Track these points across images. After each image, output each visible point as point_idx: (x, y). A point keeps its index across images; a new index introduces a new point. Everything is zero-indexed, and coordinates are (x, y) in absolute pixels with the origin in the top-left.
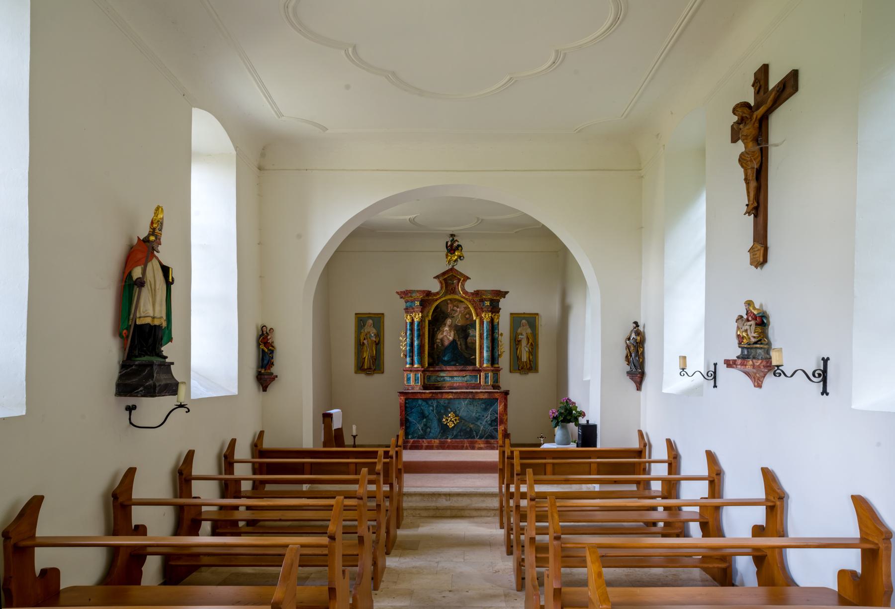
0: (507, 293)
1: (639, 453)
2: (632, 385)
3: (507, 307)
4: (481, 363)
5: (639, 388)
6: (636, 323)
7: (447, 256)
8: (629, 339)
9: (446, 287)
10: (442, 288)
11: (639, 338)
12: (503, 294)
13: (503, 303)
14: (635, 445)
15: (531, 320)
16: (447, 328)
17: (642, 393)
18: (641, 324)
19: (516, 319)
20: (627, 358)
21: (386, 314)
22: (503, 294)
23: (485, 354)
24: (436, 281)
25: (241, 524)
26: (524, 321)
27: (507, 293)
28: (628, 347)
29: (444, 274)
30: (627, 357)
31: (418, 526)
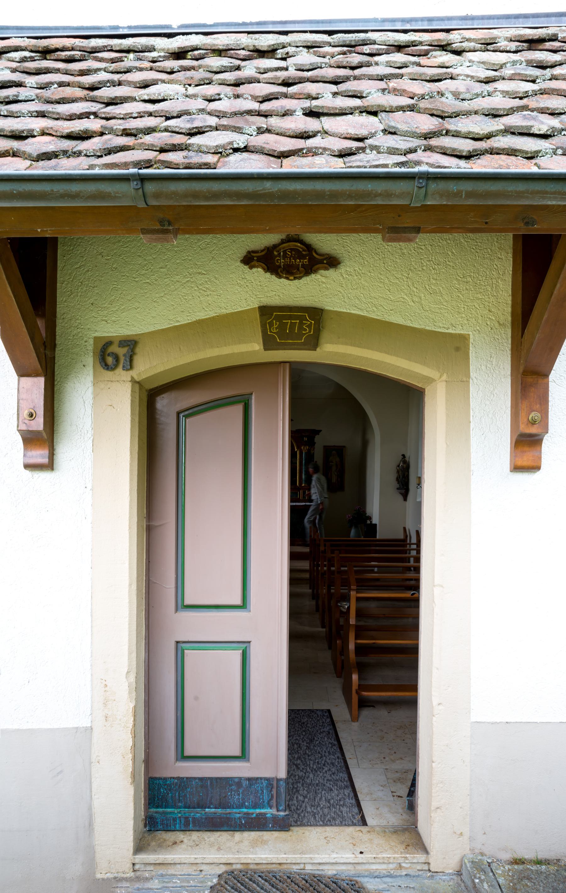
0: (321, 431)
1: (405, 540)
2: (401, 498)
3: (320, 442)
4: (301, 483)
5: (405, 499)
6: (403, 455)
8: (399, 466)
11: (405, 466)
12: (318, 432)
13: (317, 439)
14: (402, 537)
15: (340, 451)
17: (407, 503)
18: (407, 456)
19: (328, 450)
20: (397, 479)
22: (318, 432)
23: (303, 477)
24: (455, 88)
25: (343, 657)
26: (334, 452)
27: (321, 431)
28: (398, 472)
30: (397, 478)
31: (406, 573)
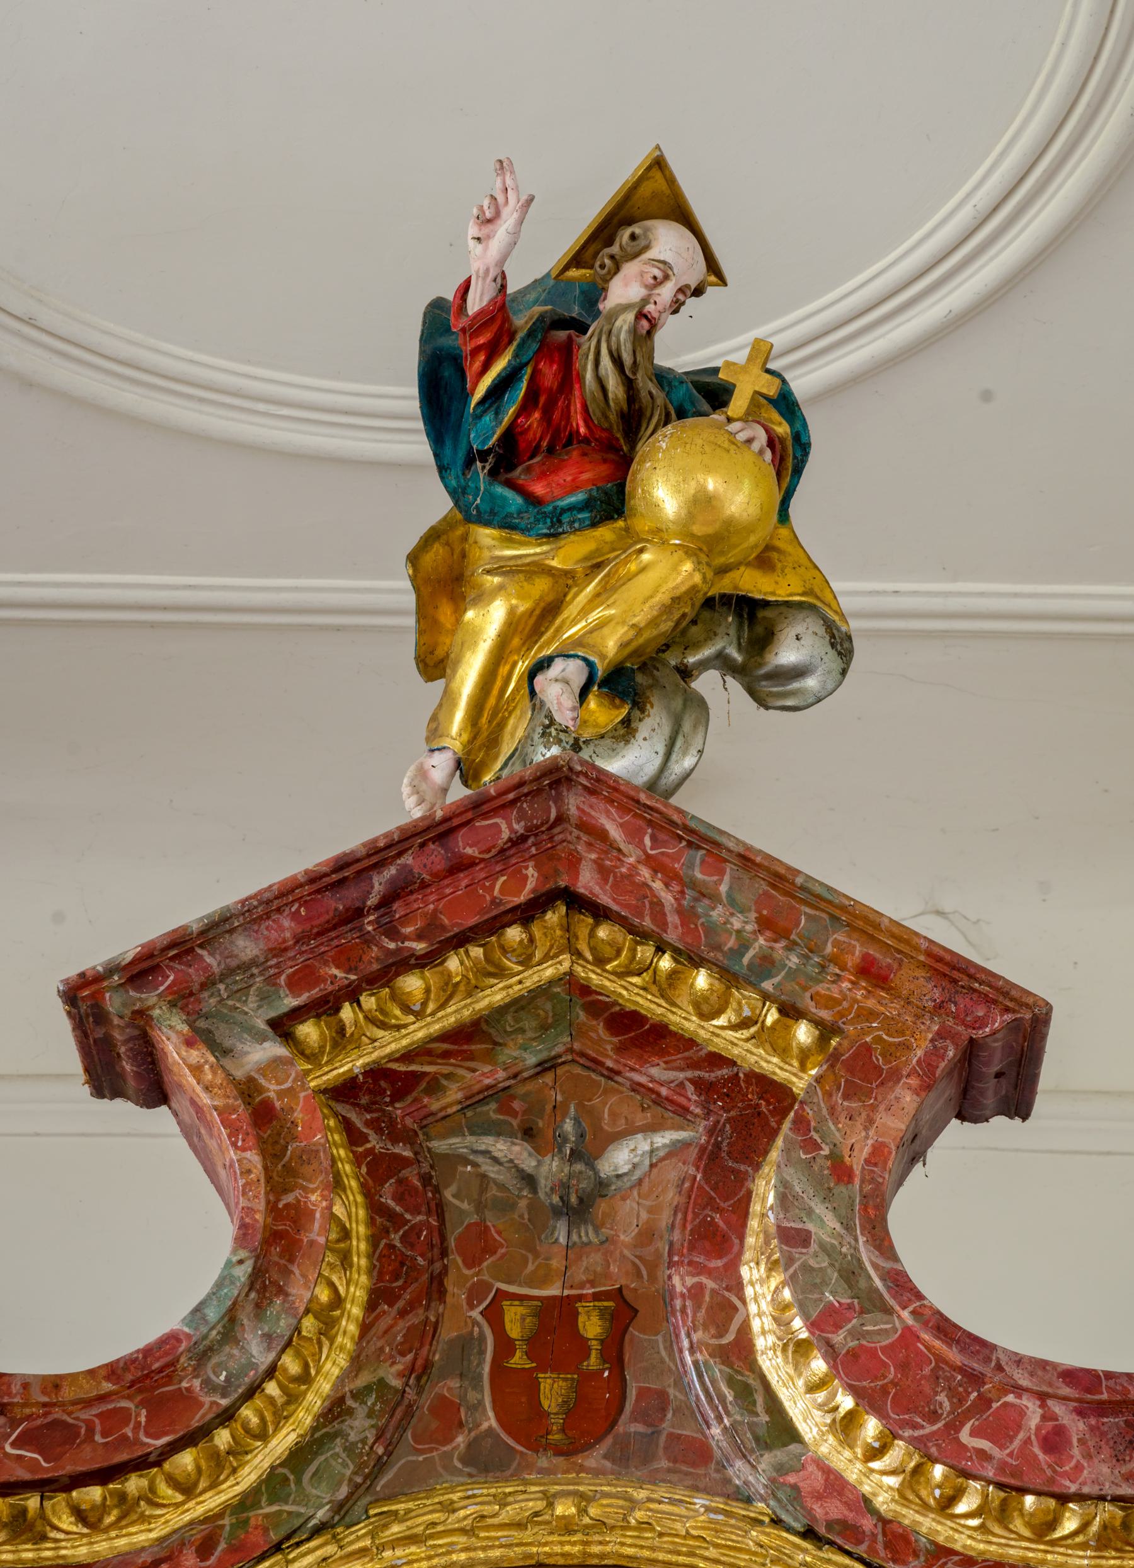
7: (443, 582)
9: (407, 1276)
10: (274, 1245)
16: (635, 1494)
29: (348, 918)
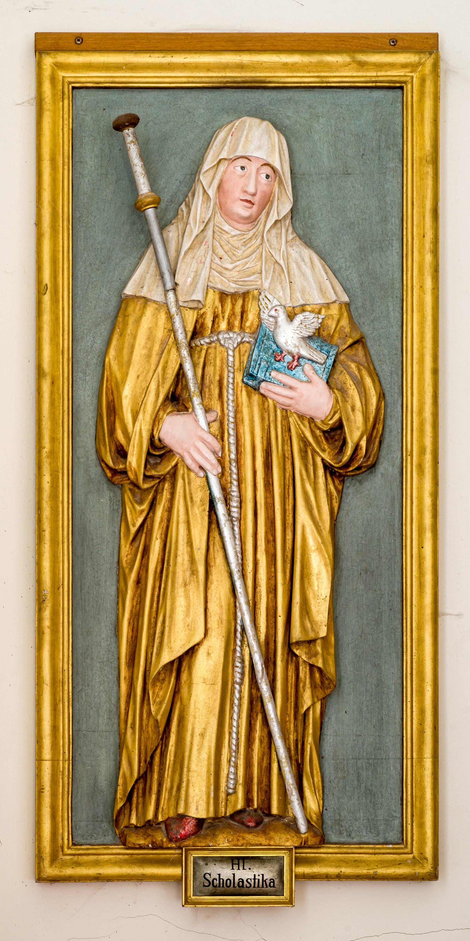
21: (452, 49)
